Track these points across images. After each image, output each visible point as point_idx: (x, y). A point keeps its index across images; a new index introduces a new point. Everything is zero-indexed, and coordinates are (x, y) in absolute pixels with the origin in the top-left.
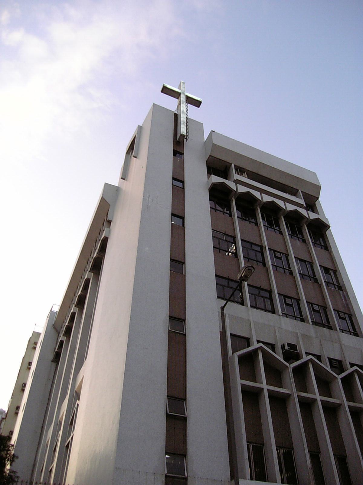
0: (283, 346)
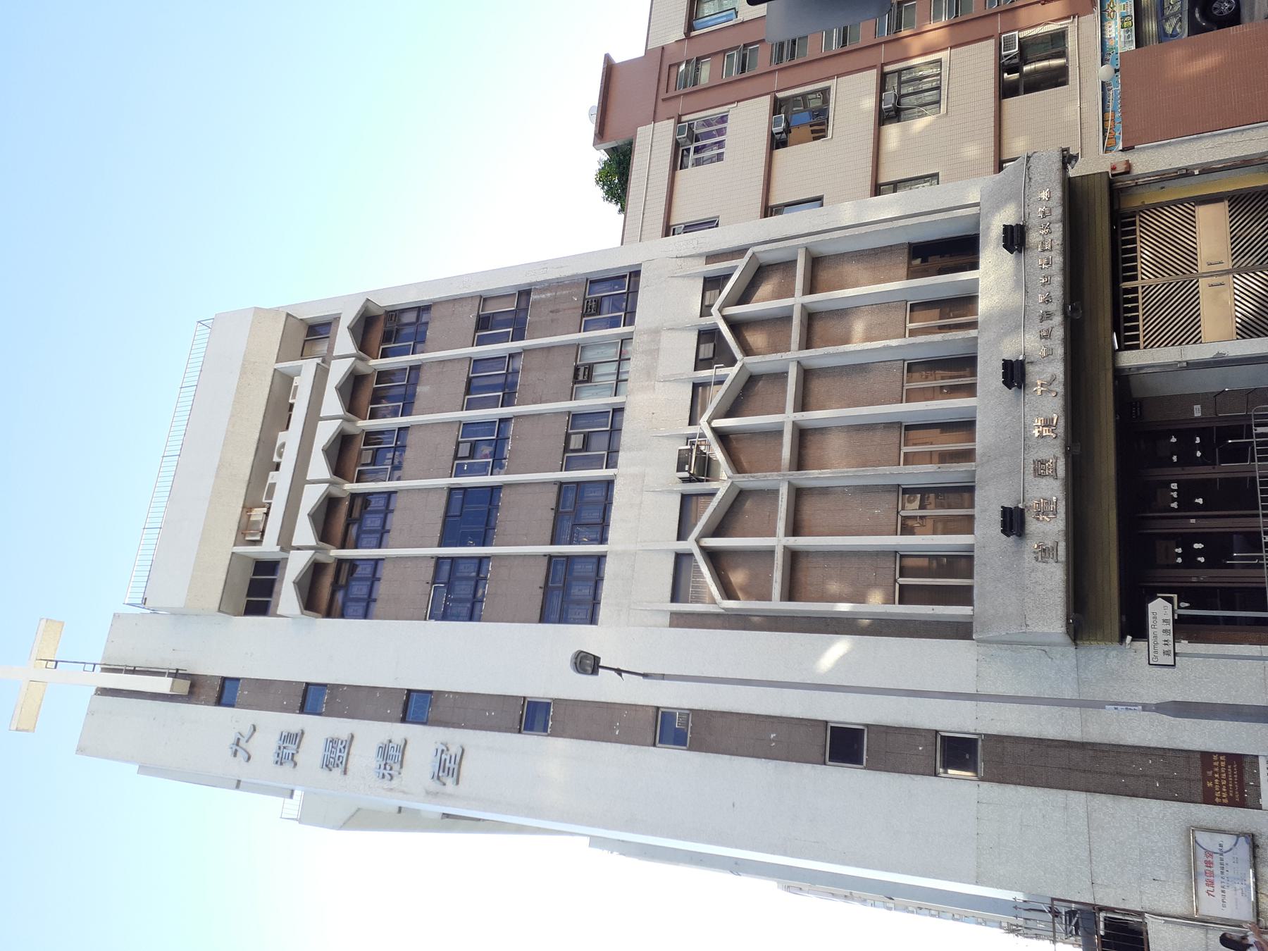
0: (684, 480)
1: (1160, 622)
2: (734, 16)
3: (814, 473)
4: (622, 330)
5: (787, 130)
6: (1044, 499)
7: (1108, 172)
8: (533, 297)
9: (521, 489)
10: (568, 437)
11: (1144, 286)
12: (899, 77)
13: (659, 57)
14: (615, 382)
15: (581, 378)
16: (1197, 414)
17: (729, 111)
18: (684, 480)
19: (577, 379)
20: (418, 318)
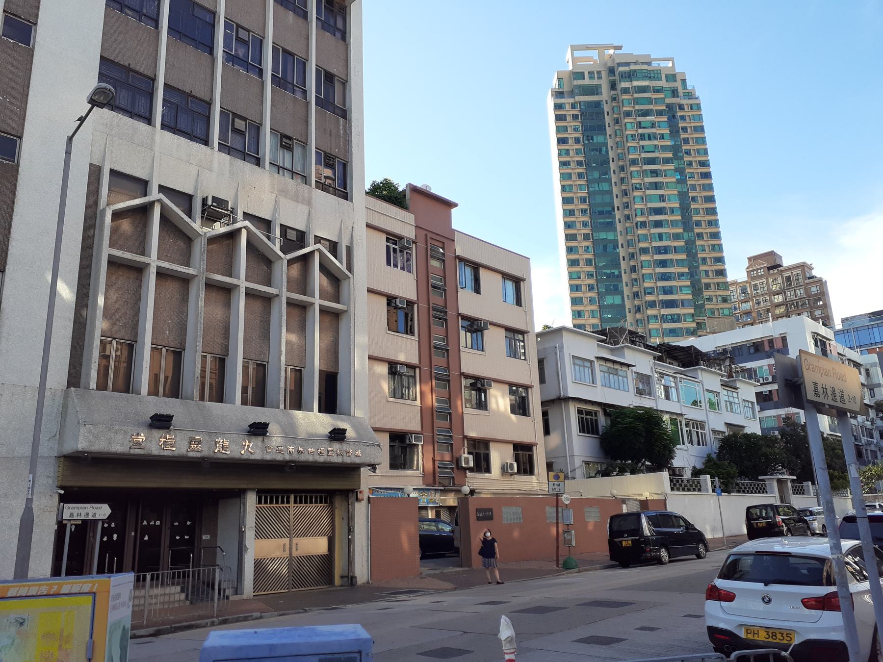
0: (205, 200)
1: (95, 511)
2: (462, 287)
3: (202, 295)
4: (313, 179)
5: (396, 307)
6: (174, 442)
7: (360, 489)
8: (342, 120)
9: (209, 71)
10: (244, 119)
12: (411, 376)
13: (447, 237)
14: (278, 164)
15: (284, 140)
16: (204, 537)
17: (413, 274)
18: (205, 200)
19: (284, 137)
20: (339, 30)
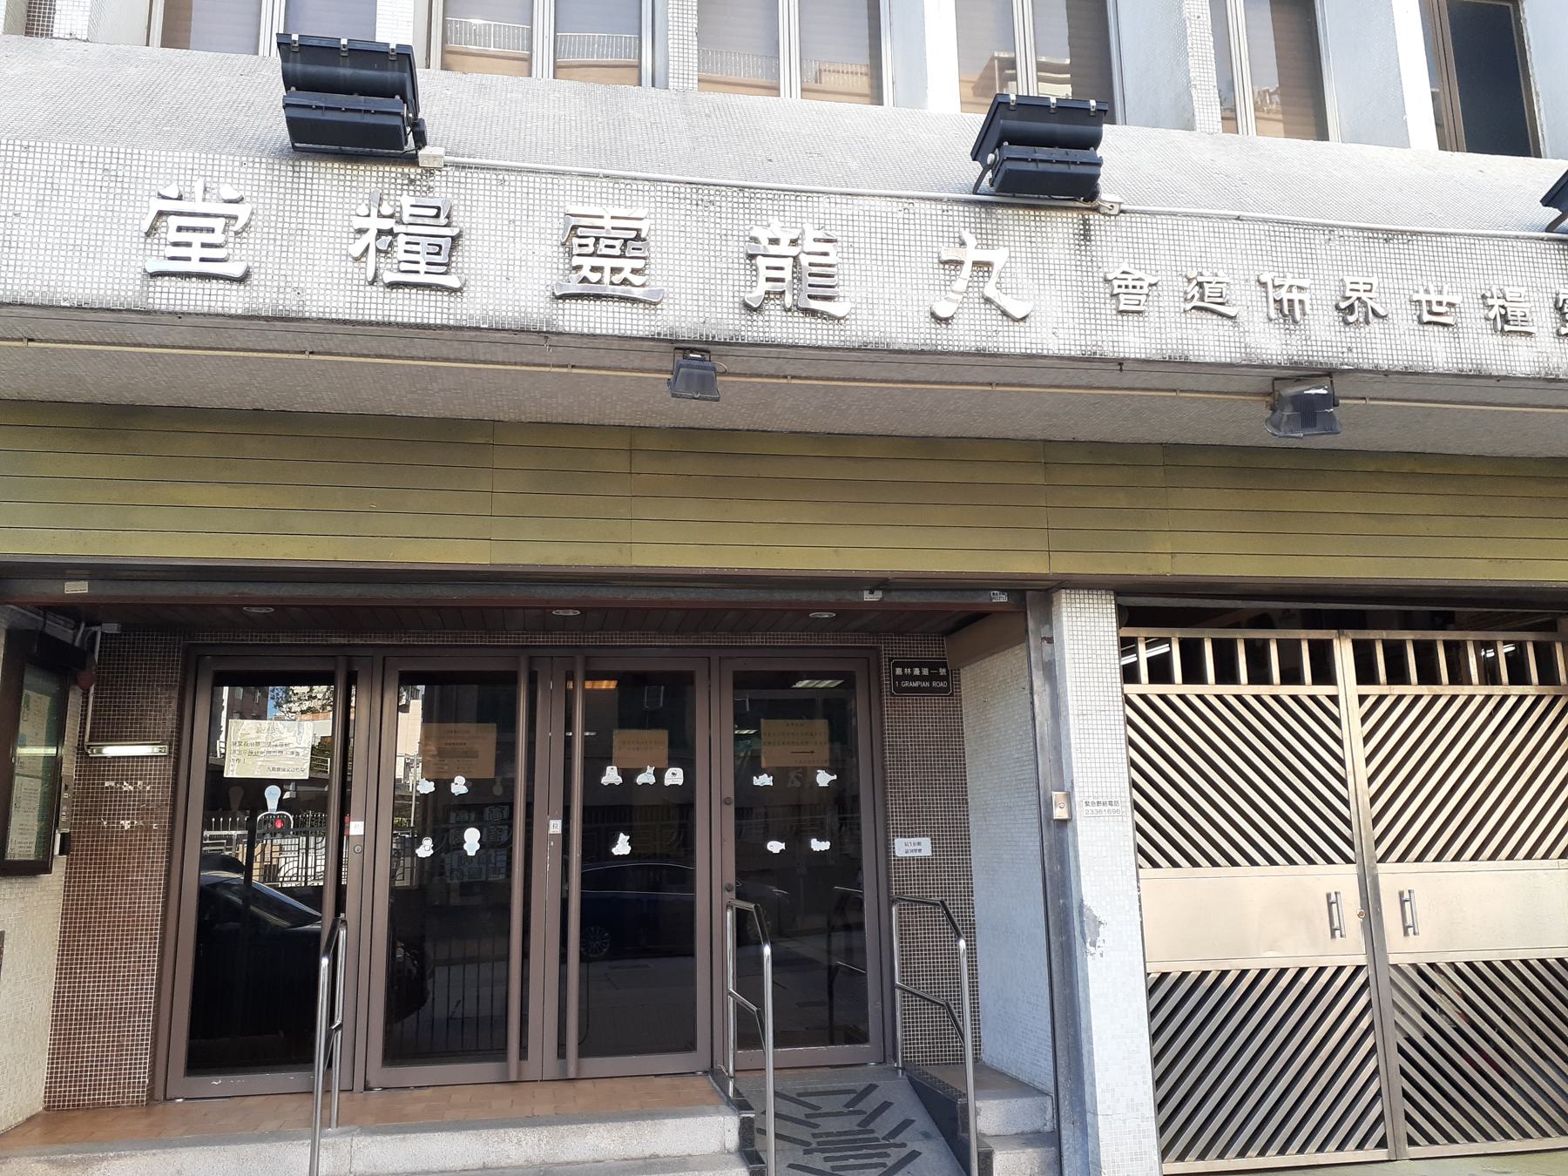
11: (1337, 704)
